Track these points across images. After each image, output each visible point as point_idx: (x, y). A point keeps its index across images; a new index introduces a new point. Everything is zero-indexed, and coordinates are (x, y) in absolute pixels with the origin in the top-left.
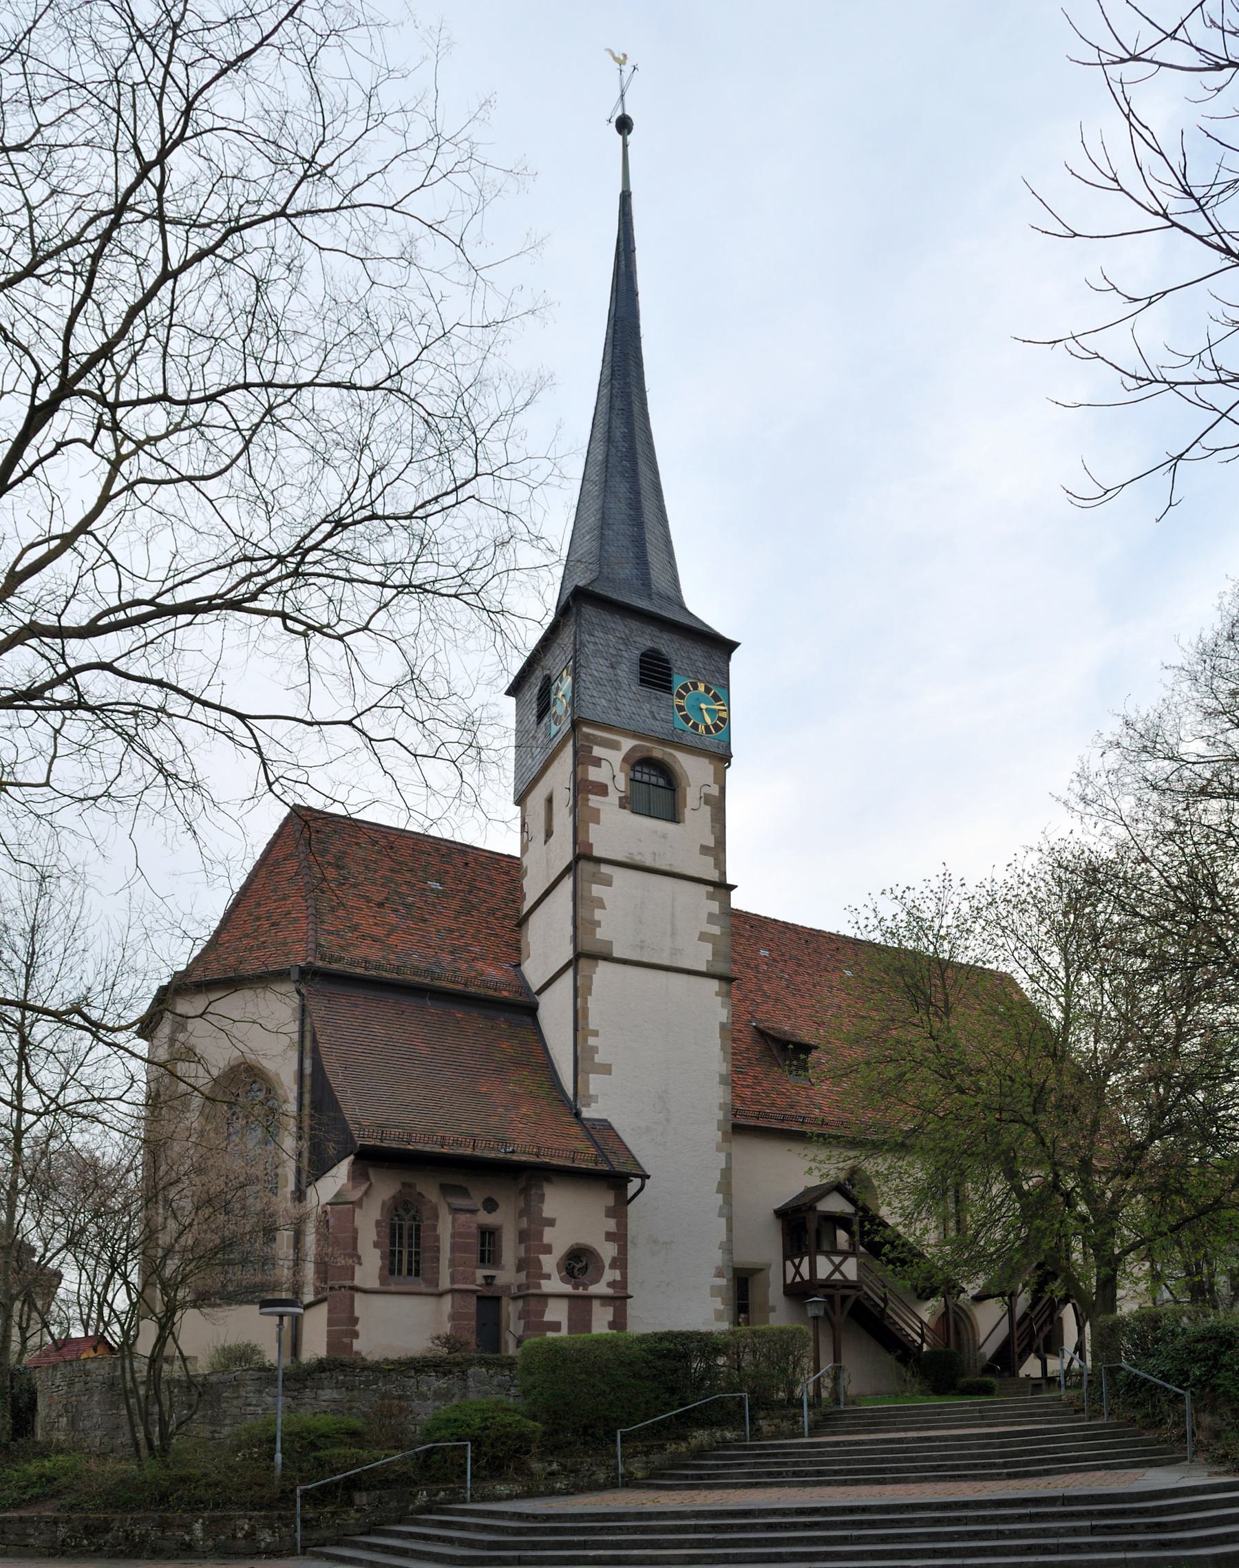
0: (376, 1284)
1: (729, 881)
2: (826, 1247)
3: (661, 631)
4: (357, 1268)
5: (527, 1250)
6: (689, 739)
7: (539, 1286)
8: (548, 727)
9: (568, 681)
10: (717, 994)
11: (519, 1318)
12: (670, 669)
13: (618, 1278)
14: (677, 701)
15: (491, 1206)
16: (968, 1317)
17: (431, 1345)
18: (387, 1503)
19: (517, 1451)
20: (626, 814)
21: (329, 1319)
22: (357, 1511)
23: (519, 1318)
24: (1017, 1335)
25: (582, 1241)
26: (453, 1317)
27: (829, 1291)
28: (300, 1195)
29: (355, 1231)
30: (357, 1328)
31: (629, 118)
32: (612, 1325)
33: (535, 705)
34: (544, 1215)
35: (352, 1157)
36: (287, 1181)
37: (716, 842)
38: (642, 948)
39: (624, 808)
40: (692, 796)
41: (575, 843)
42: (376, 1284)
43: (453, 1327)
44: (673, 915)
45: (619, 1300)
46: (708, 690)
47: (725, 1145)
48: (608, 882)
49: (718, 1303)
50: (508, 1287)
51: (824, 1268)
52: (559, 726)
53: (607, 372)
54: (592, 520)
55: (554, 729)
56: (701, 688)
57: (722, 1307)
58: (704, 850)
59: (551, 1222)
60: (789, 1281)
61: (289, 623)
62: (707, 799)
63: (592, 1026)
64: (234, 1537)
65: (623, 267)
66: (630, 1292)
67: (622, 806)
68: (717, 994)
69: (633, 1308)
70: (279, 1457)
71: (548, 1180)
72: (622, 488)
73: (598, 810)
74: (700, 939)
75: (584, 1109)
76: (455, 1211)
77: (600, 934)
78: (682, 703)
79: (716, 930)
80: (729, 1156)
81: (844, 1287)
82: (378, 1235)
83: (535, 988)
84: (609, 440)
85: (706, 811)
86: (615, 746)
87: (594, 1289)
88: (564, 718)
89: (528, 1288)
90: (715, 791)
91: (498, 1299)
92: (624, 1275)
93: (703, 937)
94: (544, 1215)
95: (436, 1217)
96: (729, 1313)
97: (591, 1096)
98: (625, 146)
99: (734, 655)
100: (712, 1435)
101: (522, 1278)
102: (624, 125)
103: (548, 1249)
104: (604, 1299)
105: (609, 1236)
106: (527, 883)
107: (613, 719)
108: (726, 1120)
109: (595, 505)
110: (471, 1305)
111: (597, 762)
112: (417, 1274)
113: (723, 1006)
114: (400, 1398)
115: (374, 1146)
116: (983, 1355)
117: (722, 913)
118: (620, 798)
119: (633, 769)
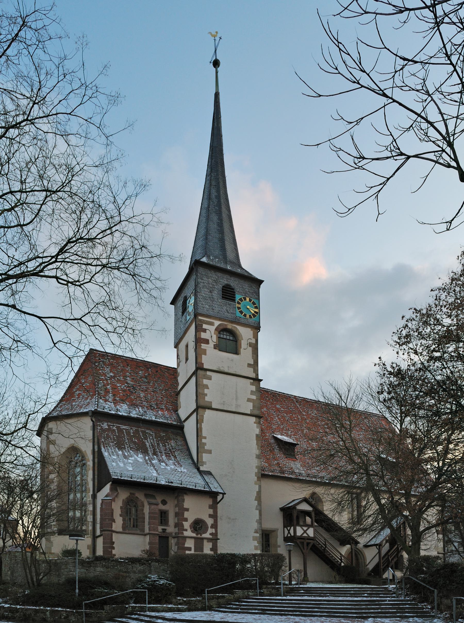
0: (121, 530)
1: (259, 378)
2: (301, 523)
3: (231, 277)
4: (113, 523)
5: (178, 520)
6: (242, 321)
7: (183, 533)
8: (186, 317)
9: (193, 298)
10: (255, 423)
11: (176, 545)
12: (234, 292)
13: (214, 532)
14: (237, 305)
15: (164, 502)
16: (361, 553)
17: (141, 553)
18: (116, 610)
19: (166, 594)
20: (217, 351)
21: (103, 542)
22: (105, 612)
23: (176, 545)
24: (382, 561)
25: (196, 518)
26: (150, 543)
27: (302, 540)
28: (94, 497)
29: (113, 510)
30: (114, 546)
31: (218, 60)
32: (211, 550)
33: (181, 308)
34: (184, 507)
35: (111, 483)
36: (90, 490)
37: (254, 362)
38: (224, 404)
39: (216, 349)
40: (244, 344)
41: (196, 363)
42: (121, 530)
43: (150, 547)
44: (236, 391)
45: (214, 539)
46: (250, 300)
47: (258, 482)
48: (210, 378)
49: (256, 543)
50: (171, 533)
51: (299, 531)
52: (189, 317)
53: (209, 170)
54: (203, 232)
55: (188, 317)
56: (248, 299)
57: (257, 545)
58: (249, 365)
59: (187, 510)
60: (286, 536)
61: (60, 281)
62: (250, 345)
63: (204, 435)
64: (60, 618)
65: (216, 125)
66: (219, 537)
67: (215, 348)
68: (255, 423)
69: (220, 544)
70: (77, 591)
71: (186, 494)
72: (215, 218)
73: (206, 350)
74: (247, 401)
75: (201, 467)
76: (150, 504)
77: (207, 399)
78: (239, 306)
79: (254, 397)
80: (260, 487)
81: (308, 539)
82: (121, 512)
83: (183, 420)
84: (209, 198)
85: (250, 349)
86: (212, 324)
87: (204, 536)
88: (192, 313)
89: (179, 534)
90: (253, 341)
91: (168, 538)
92: (216, 531)
93: (249, 400)
94: (184, 507)
95: (143, 506)
96: (260, 547)
97: (203, 462)
98: (217, 72)
99: (262, 286)
100: (244, 593)
101: (176, 530)
102: (216, 63)
103: (186, 520)
104: (209, 540)
105: (210, 516)
106: (179, 379)
107: (211, 313)
108: (258, 472)
109: (203, 226)
110: (157, 539)
111: (205, 331)
112: (137, 527)
113: (257, 428)
114: (125, 572)
115: (118, 478)
116: (368, 568)
117: (256, 390)
118: (214, 345)
119: (219, 333)
